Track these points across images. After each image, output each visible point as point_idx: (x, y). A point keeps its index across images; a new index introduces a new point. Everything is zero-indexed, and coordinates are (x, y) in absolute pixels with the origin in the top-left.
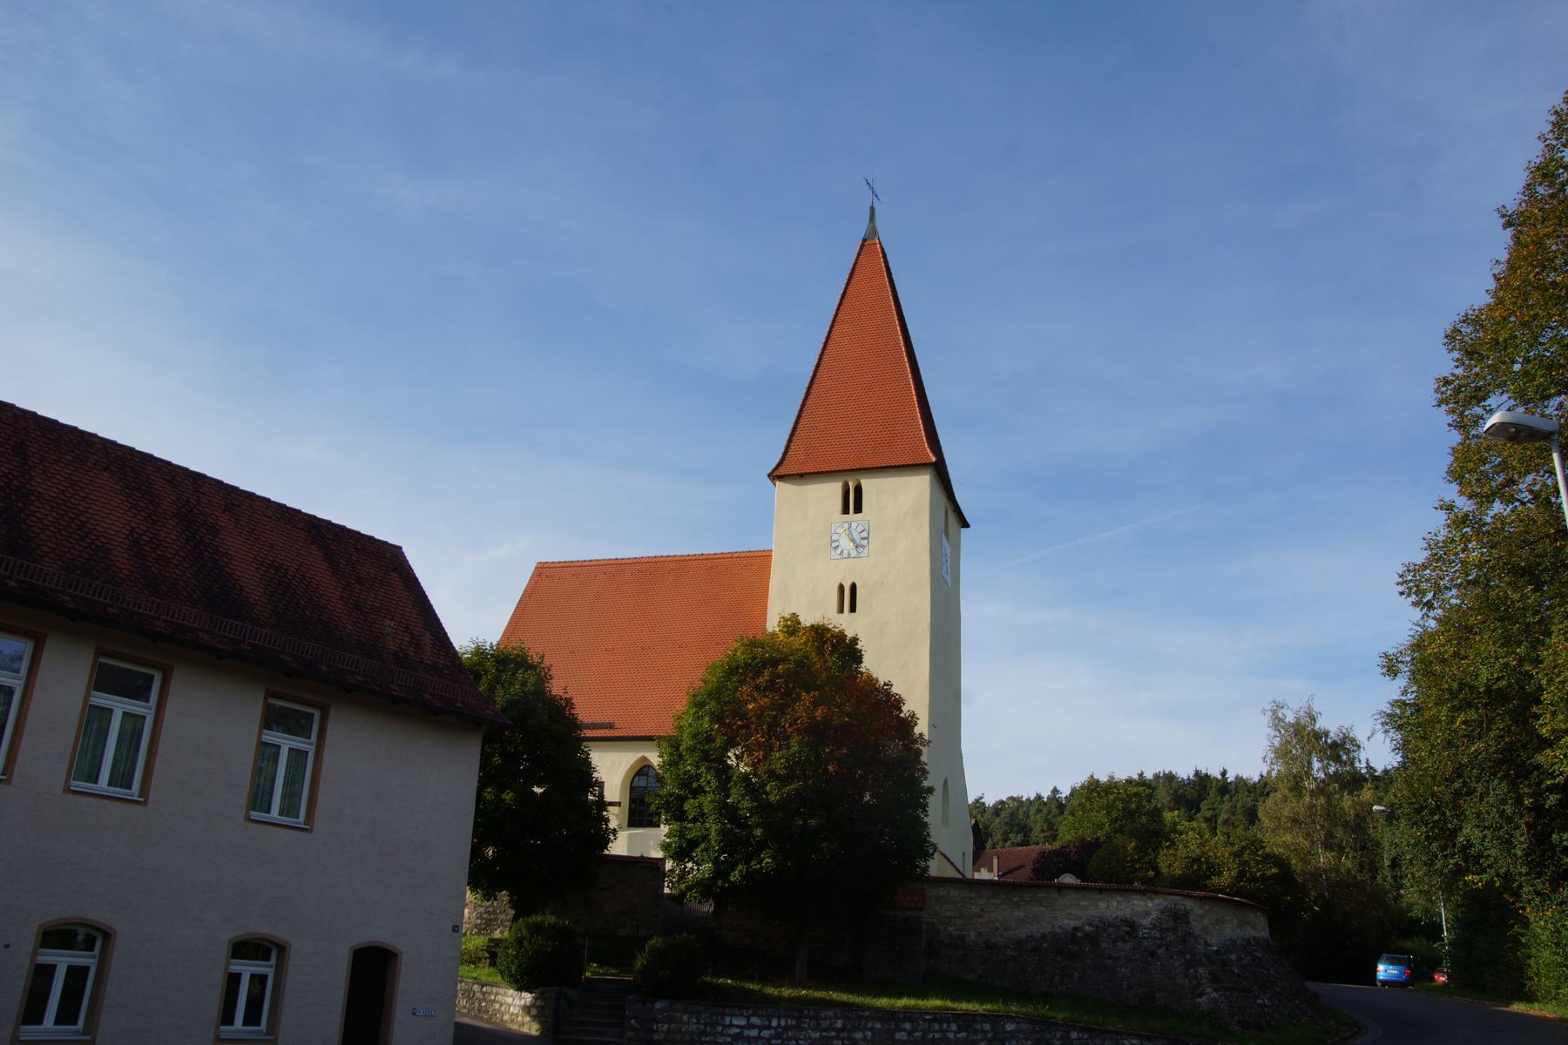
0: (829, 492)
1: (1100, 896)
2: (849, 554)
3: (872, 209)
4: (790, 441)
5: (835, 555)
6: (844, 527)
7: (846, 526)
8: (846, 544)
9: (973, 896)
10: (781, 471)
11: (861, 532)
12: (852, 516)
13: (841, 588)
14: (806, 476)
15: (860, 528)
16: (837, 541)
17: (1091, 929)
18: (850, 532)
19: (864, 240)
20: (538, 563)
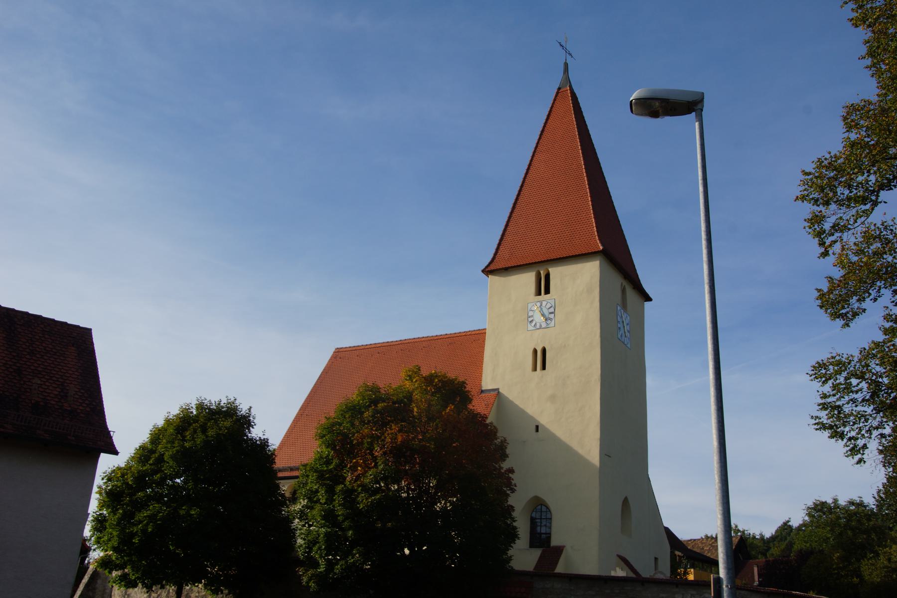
0: (527, 279)
2: (541, 325)
3: (566, 65)
4: (499, 244)
5: (531, 327)
6: (536, 306)
7: (538, 304)
8: (539, 319)
9: (572, 588)
10: (492, 267)
11: (549, 308)
12: (543, 297)
13: (535, 351)
14: (509, 269)
16: (532, 316)
18: (541, 309)
19: (559, 89)
20: (336, 349)
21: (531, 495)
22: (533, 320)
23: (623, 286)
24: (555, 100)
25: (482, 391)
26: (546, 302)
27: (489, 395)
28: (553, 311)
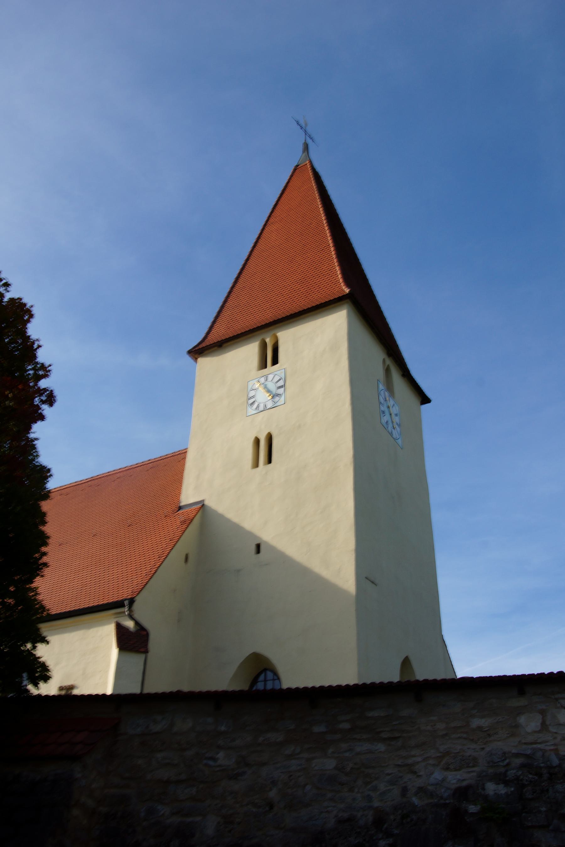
1: (521, 702)
5: (252, 411)
8: (262, 397)
12: (270, 369)
14: (225, 345)
15: (277, 378)
16: (253, 397)
17: (502, 790)
21: (246, 652)
22: (254, 402)
23: (386, 365)
24: (292, 176)
25: (180, 508)
26: (273, 375)
27: (190, 510)
28: (283, 384)
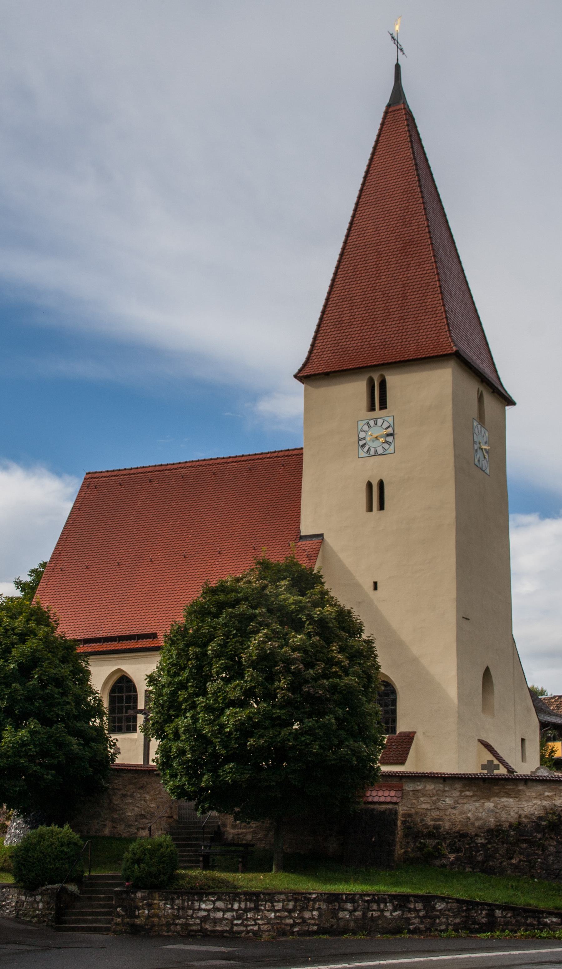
12: (378, 413)
15: (386, 425)
16: (364, 439)
22: (365, 444)
